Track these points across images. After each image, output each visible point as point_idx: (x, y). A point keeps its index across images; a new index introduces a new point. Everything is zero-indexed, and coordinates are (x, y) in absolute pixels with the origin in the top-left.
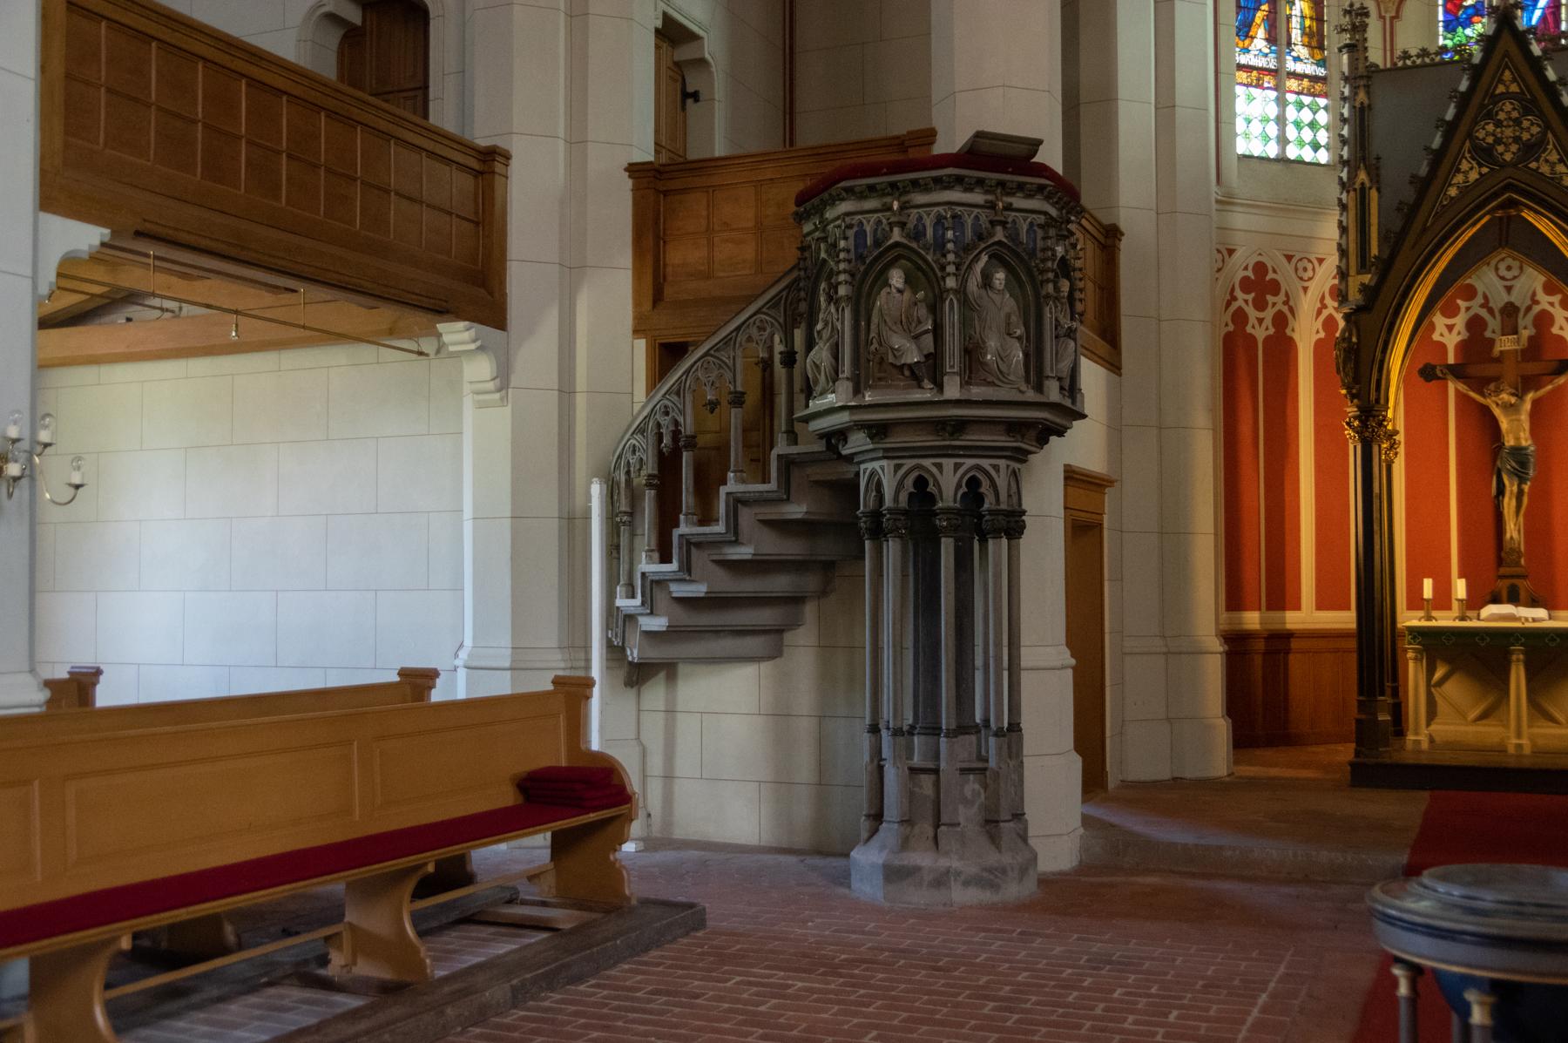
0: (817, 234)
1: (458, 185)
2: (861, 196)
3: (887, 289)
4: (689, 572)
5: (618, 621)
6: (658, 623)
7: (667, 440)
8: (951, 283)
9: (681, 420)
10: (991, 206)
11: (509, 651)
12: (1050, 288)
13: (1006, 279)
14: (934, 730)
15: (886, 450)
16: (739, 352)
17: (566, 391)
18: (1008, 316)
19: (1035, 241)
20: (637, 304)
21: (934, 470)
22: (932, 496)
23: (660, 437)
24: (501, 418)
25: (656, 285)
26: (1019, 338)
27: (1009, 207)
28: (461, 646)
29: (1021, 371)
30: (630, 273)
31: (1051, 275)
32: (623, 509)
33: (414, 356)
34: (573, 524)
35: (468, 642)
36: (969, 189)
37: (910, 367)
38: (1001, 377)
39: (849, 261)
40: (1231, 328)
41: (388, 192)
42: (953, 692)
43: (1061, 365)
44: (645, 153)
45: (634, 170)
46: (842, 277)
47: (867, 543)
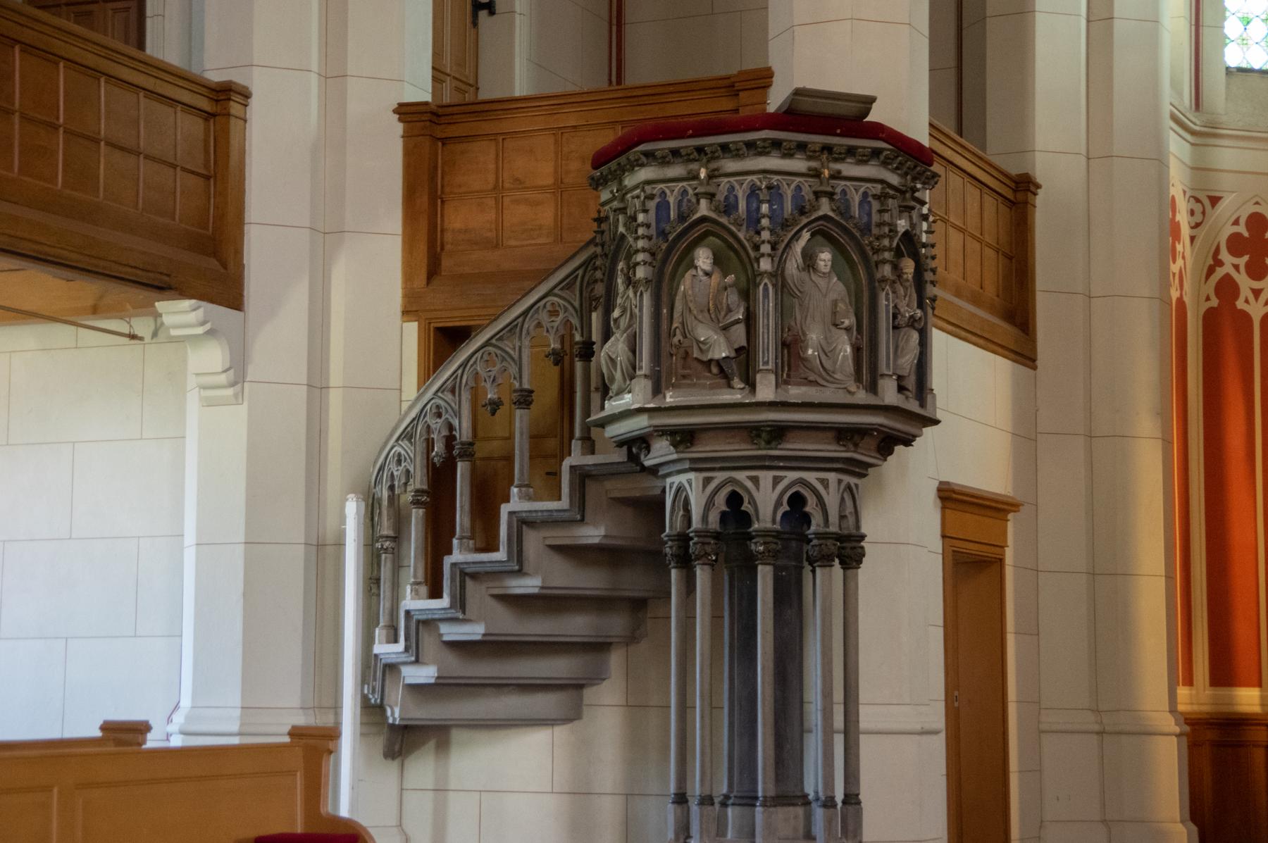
0: (615, 204)
1: (185, 131)
2: (663, 162)
3: (692, 272)
4: (463, 608)
5: (377, 672)
6: (425, 674)
7: (439, 448)
8: (765, 265)
9: (456, 423)
10: (816, 174)
11: (238, 712)
12: (887, 270)
13: (834, 261)
14: (749, 800)
15: (692, 460)
16: (526, 342)
17: (317, 387)
18: (835, 303)
19: (869, 215)
20: (408, 277)
21: (749, 484)
22: (746, 514)
23: (430, 444)
24: (235, 419)
25: (430, 255)
26: (848, 329)
27: (837, 176)
28: (177, 707)
29: (850, 367)
30: (399, 240)
31: (887, 255)
32: (385, 532)
33: (126, 340)
34: (324, 553)
35: (186, 702)
36: (788, 155)
37: (718, 362)
38: (826, 376)
39: (650, 238)
40: (1215, 302)
41: (97, 141)
42: (771, 753)
43: (901, 361)
44: (420, 90)
45: (406, 112)
46: (640, 257)
47: (674, 573)
